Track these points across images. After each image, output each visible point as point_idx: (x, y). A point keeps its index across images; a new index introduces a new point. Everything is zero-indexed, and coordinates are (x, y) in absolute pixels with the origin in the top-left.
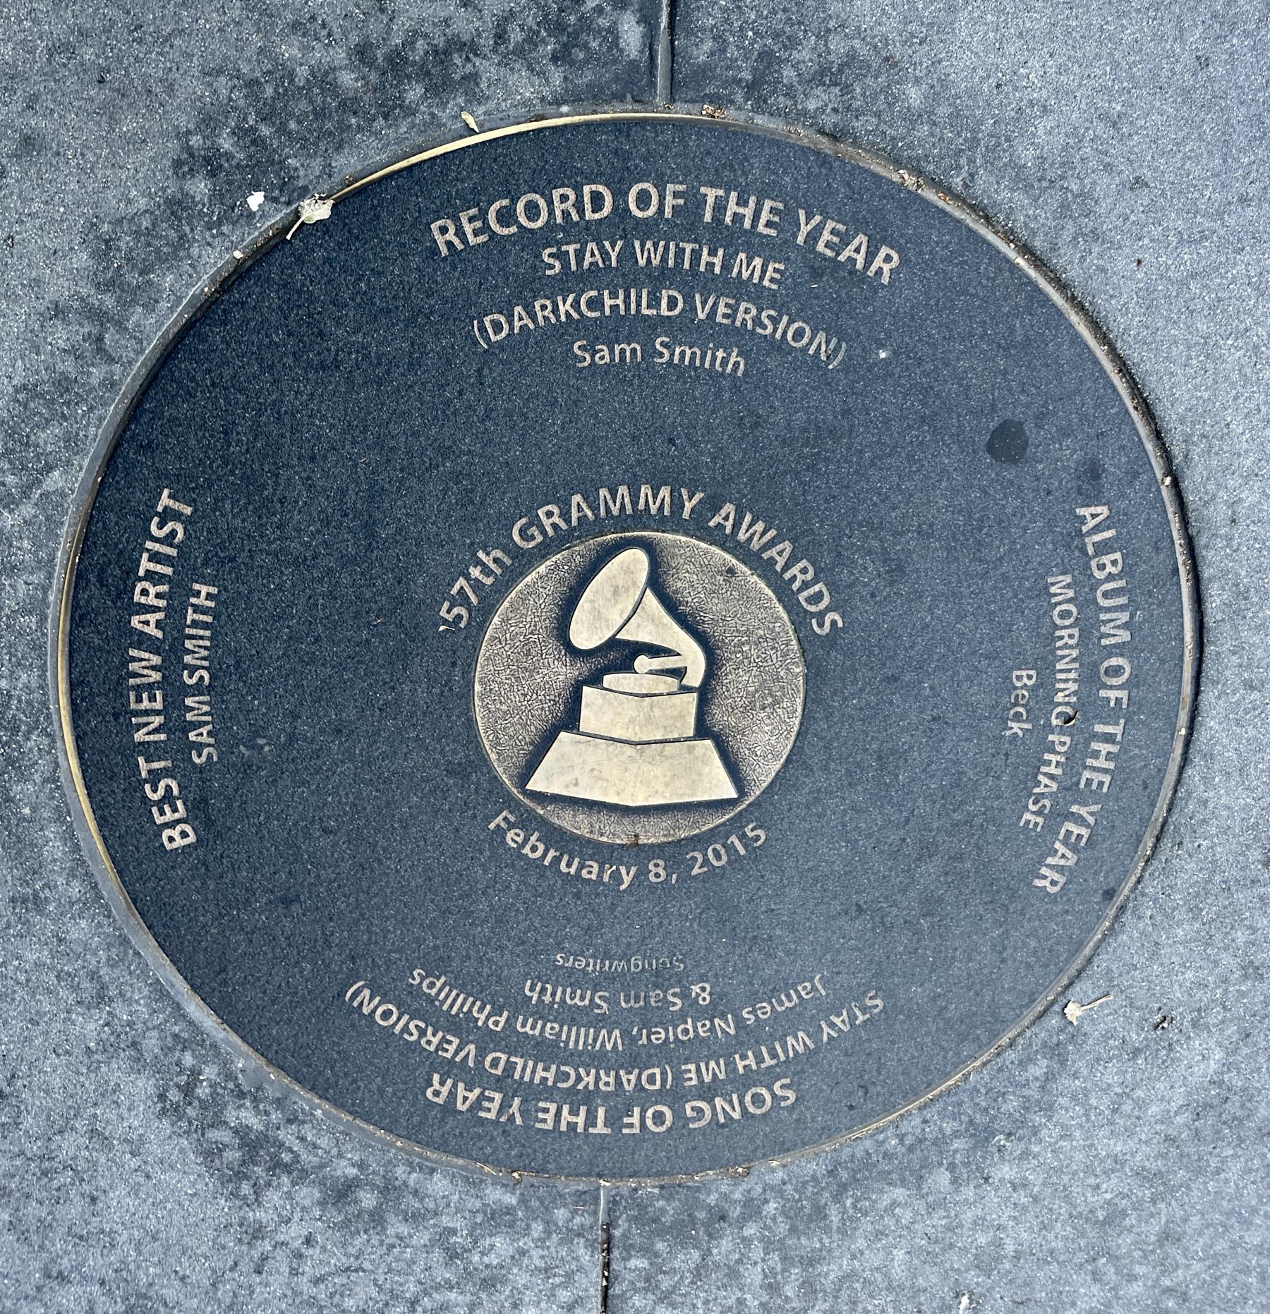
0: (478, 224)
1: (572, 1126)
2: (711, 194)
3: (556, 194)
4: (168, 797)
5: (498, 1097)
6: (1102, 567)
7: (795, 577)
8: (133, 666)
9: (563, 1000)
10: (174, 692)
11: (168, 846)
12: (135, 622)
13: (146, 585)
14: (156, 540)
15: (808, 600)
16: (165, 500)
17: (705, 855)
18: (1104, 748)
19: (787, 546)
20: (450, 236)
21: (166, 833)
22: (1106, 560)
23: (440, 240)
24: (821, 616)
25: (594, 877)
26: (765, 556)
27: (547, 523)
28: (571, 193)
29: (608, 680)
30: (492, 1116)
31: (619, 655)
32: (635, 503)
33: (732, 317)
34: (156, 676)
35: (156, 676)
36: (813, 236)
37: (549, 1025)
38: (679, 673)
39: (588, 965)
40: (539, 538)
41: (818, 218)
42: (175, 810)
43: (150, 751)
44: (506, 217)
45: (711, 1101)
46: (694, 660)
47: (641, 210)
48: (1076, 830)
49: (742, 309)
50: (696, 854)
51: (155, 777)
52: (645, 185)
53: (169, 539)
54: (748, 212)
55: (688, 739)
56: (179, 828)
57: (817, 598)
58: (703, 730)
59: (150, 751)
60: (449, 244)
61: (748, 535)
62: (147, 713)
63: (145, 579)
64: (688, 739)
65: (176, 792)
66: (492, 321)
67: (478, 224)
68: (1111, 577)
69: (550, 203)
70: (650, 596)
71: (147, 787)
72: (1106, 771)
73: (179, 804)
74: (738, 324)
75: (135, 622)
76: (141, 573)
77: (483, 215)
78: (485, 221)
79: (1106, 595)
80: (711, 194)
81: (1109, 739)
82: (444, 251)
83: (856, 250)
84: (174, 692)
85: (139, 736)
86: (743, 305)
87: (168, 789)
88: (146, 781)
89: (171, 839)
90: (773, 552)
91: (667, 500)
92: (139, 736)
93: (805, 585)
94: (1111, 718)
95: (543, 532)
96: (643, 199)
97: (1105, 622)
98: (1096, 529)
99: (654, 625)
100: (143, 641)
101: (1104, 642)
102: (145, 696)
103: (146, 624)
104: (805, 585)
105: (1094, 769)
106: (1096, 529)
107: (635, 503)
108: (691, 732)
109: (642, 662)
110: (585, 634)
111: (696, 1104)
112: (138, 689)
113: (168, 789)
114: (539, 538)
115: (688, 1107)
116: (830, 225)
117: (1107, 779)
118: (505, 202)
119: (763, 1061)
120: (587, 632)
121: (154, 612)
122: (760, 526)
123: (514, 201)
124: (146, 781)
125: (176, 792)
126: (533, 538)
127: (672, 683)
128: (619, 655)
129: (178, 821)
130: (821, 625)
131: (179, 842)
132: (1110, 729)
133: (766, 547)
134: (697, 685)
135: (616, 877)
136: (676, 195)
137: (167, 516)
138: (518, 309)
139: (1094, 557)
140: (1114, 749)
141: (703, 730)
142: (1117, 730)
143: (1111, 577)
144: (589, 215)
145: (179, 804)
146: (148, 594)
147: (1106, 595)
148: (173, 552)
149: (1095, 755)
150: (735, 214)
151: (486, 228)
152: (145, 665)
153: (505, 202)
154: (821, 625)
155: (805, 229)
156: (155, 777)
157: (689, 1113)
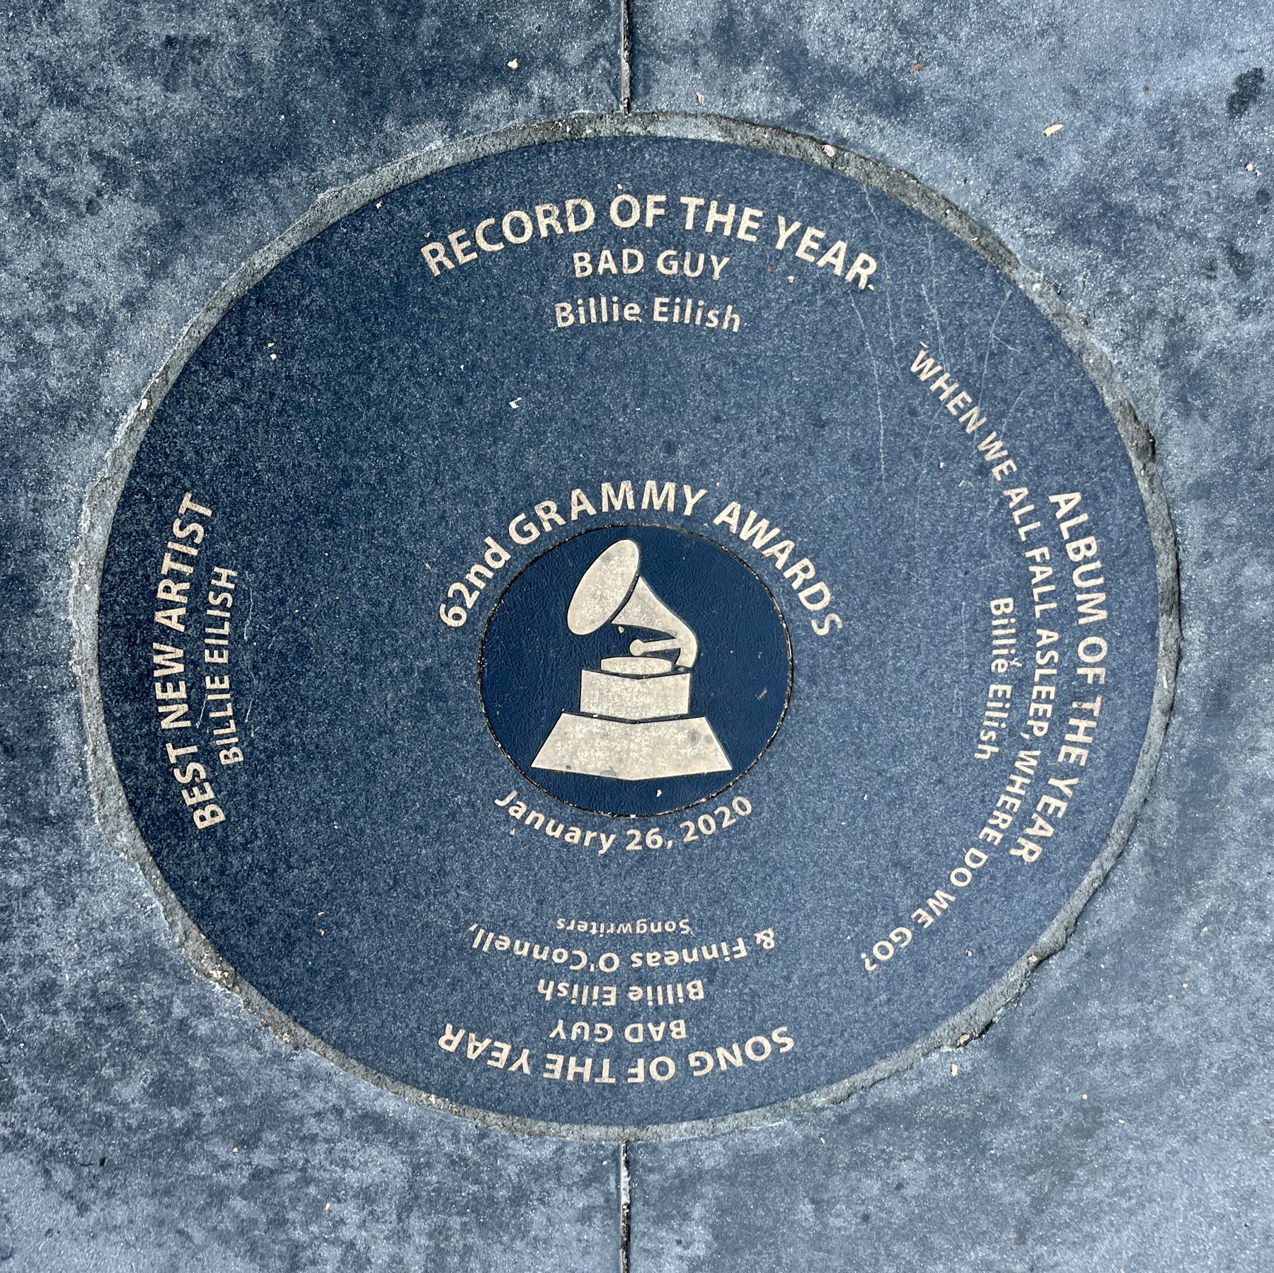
0: (467, 244)
2: (692, 203)
3: (539, 210)
6: (1077, 551)
7: (796, 576)
10: (195, 671)
13: (169, 582)
16: (186, 503)
17: (732, 810)
22: (1081, 543)
23: (432, 264)
25: (518, 816)
29: (606, 664)
31: (614, 639)
32: (638, 501)
34: (179, 668)
35: (179, 668)
36: (794, 241)
37: (518, 816)
38: (672, 655)
39: (590, 927)
40: (536, 534)
41: (513, 1068)
43: (181, 738)
44: (494, 235)
45: (712, 1051)
46: (688, 644)
48: (1054, 803)
50: (688, 823)
51: (183, 762)
54: (729, 219)
55: (682, 717)
56: (210, 808)
58: (695, 710)
59: (181, 738)
60: (440, 265)
62: (174, 701)
64: (682, 717)
65: (203, 775)
67: (467, 244)
68: (1087, 561)
69: (534, 220)
70: (641, 583)
72: (1083, 745)
75: (159, 617)
76: (164, 571)
77: (470, 236)
79: (1086, 576)
80: (692, 203)
83: (835, 257)
85: (166, 724)
88: (175, 766)
89: (203, 819)
90: (774, 550)
92: (166, 724)
93: (806, 584)
95: (540, 527)
96: (625, 212)
97: (1082, 603)
98: (1021, 505)
99: (649, 609)
100: (166, 634)
102: (169, 685)
103: (171, 619)
104: (806, 584)
105: (1073, 744)
106: (1021, 505)
107: (638, 501)
108: (685, 711)
109: (637, 646)
110: (584, 616)
111: (698, 1054)
112: (166, 678)
114: (536, 534)
115: (692, 1057)
116: (811, 231)
118: (491, 221)
120: (584, 616)
121: (845, 263)
123: (500, 219)
124: (175, 766)
126: (697, 1059)
127: (666, 665)
128: (614, 639)
129: (210, 802)
131: (578, 264)
134: (690, 665)
135: (596, 842)
136: (657, 205)
137: (192, 517)
138: (841, 246)
141: (695, 710)
143: (1087, 561)
144: (573, 228)
146: (172, 592)
147: (1086, 576)
148: (194, 552)
150: (716, 222)
151: (474, 248)
152: (169, 659)
153: (491, 221)
155: (784, 235)
156: (183, 762)
157: (693, 1063)
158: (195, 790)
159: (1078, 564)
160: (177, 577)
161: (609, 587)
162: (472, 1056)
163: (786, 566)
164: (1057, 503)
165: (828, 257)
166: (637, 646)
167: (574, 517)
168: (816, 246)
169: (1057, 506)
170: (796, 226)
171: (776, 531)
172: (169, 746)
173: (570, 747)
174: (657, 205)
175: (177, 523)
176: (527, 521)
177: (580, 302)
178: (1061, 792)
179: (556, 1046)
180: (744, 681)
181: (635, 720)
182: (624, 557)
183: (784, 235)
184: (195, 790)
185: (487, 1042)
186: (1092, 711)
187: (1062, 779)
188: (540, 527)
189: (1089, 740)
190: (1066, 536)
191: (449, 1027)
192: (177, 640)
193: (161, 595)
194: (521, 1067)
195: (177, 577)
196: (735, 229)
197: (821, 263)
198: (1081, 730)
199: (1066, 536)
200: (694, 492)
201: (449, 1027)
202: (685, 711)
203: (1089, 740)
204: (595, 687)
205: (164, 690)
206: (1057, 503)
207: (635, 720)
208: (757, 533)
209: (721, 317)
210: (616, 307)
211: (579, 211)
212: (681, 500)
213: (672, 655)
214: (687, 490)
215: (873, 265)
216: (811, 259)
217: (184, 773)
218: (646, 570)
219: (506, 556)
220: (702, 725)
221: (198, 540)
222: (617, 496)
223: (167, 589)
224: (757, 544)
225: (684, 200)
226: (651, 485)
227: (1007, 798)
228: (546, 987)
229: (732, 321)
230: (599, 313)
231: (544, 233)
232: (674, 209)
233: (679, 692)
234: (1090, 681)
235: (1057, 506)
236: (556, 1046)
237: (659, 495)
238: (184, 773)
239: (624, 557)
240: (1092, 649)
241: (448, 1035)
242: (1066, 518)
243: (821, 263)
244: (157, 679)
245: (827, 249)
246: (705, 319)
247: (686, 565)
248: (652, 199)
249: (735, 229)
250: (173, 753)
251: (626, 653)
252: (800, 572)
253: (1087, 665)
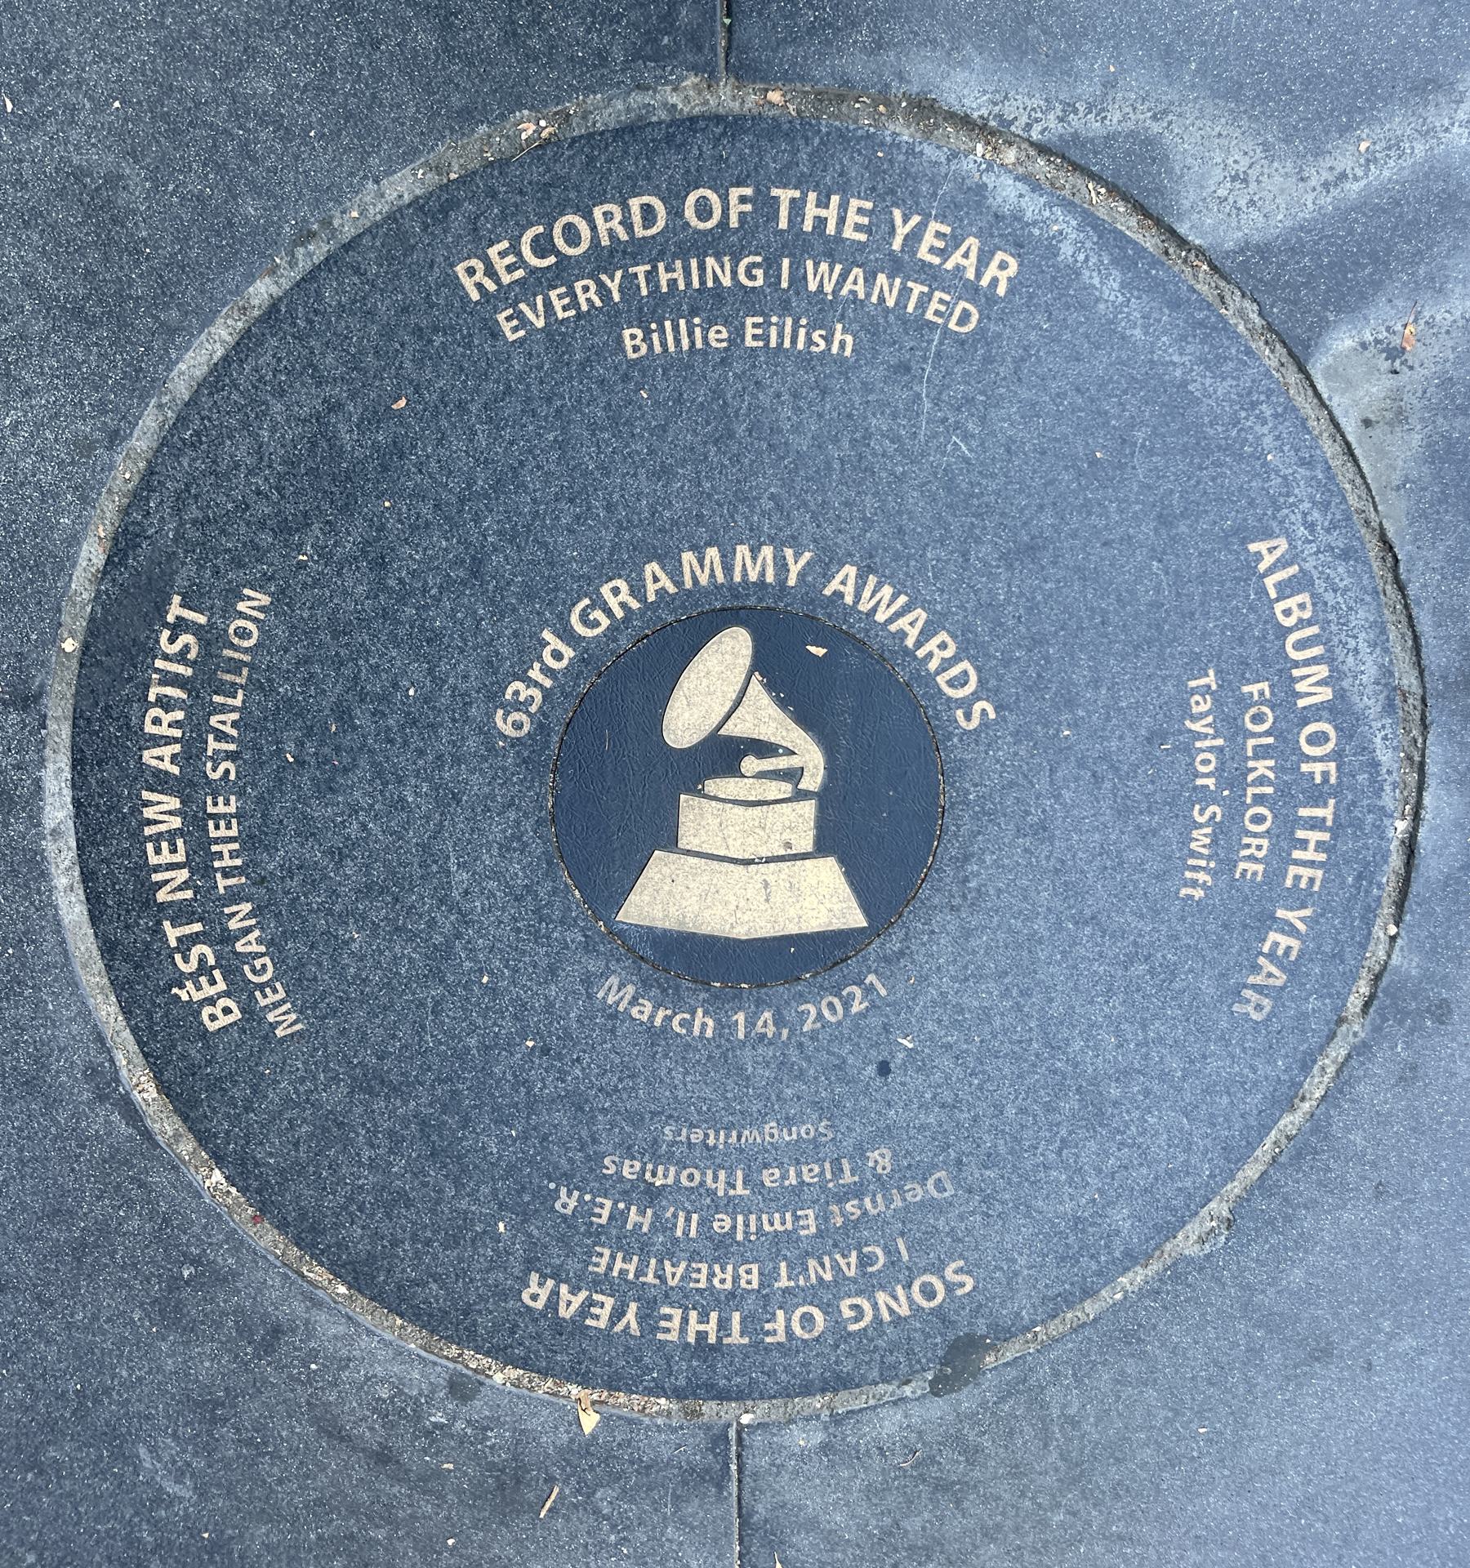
1: (701, 1336)
3: (598, 212)
4: (203, 968)
5: (609, 1302)
8: (149, 813)
9: (760, 1228)
10: (195, 822)
11: (212, 1027)
12: (148, 756)
14: (166, 657)
15: (951, 683)
16: (175, 611)
18: (1314, 836)
19: (921, 615)
20: (479, 276)
21: (206, 1011)
23: (468, 283)
24: (967, 704)
26: (893, 628)
27: (613, 603)
28: (616, 209)
29: (712, 786)
30: (602, 1324)
31: (723, 754)
33: (574, 303)
35: (176, 822)
36: (914, 237)
38: (793, 775)
40: (605, 622)
42: (213, 982)
46: (811, 758)
47: (700, 219)
49: (579, 291)
51: (186, 944)
52: (701, 192)
53: (181, 657)
57: (960, 681)
58: (822, 848)
59: (182, 912)
61: (707, 562)
63: (155, 705)
64: (804, 856)
65: (211, 961)
66: (965, 673)
68: (1302, 624)
71: (178, 957)
72: (217, 841)
73: (217, 974)
74: (584, 307)
75: (148, 756)
77: (515, 249)
78: (519, 254)
79: (1300, 645)
80: (785, 195)
81: (1316, 824)
82: (475, 296)
84: (195, 822)
85: (162, 896)
86: (578, 286)
87: (202, 960)
89: (213, 1018)
90: (902, 623)
91: (770, 561)
94: (1318, 800)
95: (609, 612)
99: (762, 717)
100: (161, 782)
101: (1301, 703)
102: (164, 845)
103: (160, 758)
108: (810, 849)
109: (750, 764)
110: (687, 718)
112: (157, 839)
113: (202, 960)
114: (605, 622)
117: (1319, 874)
119: (226, 875)
122: (887, 591)
125: (211, 961)
127: (784, 789)
129: (220, 996)
130: (968, 716)
131: (224, 1021)
132: (1319, 812)
133: (891, 620)
136: (743, 200)
137: (180, 626)
139: (1278, 600)
140: (1325, 836)
141: (822, 848)
142: (1326, 813)
143: (1302, 624)
145: (217, 974)
146: (161, 723)
147: (1300, 645)
149: (1303, 844)
151: (521, 262)
152: (162, 810)
153: (541, 229)
154: (968, 716)
155: (902, 231)
156: (186, 944)
158: (203, 980)
159: (1290, 630)
160: (165, 704)
161: (717, 686)
162: (565, 1313)
163: (919, 644)
164: (1259, 552)
165: (956, 259)
166: (750, 764)
167: (651, 598)
168: (940, 244)
169: (1259, 557)
170: (916, 219)
171: (902, 600)
172: (167, 924)
173: (670, 895)
174: (743, 200)
175: (166, 634)
176: (593, 606)
177: (653, 326)
178: (1291, 925)
179: (1275, 874)
180: (888, 807)
181: (746, 864)
182: (731, 650)
183: (902, 231)
184: (203, 980)
185: (583, 1295)
186: (1324, 819)
187: (1292, 909)
188: (609, 612)
189: (1322, 857)
190: (1273, 594)
191: (1001, 290)
192: (161, 782)
193: (149, 728)
194: (628, 1326)
195: (165, 704)
196: (842, 221)
197: (949, 265)
198: (1312, 845)
199: (1273, 594)
200: (797, 556)
201: (1001, 290)
202: (810, 849)
203: (1322, 857)
204: (701, 820)
205: (158, 851)
206: (1259, 552)
207: (746, 864)
208: (881, 602)
209: (828, 339)
210: (698, 331)
211: (648, 212)
212: (782, 566)
213: (793, 775)
214: (789, 553)
215: (1013, 265)
216: (936, 260)
217: (186, 960)
218: (759, 663)
219: (568, 653)
220: (831, 862)
221: (192, 656)
222: (702, 566)
223: (157, 721)
224: (880, 617)
225: (775, 192)
226: (743, 551)
227: (1301, 871)
228: (704, 1025)
229: (704, 1025)
230: (677, 341)
231: (605, 242)
232: (766, 206)
233: (798, 823)
234: (1318, 780)
235: (1259, 557)
236: (1275, 874)
237: (754, 564)
238: (186, 960)
239: (731, 650)
240: (1317, 739)
241: (534, 1288)
242: (1270, 571)
243: (949, 265)
244: (150, 838)
245: (957, 247)
246: (810, 341)
247: (804, 655)
248: (735, 193)
249: (842, 221)
250: (172, 934)
251: (734, 771)
252: (938, 649)
253: (1315, 759)
